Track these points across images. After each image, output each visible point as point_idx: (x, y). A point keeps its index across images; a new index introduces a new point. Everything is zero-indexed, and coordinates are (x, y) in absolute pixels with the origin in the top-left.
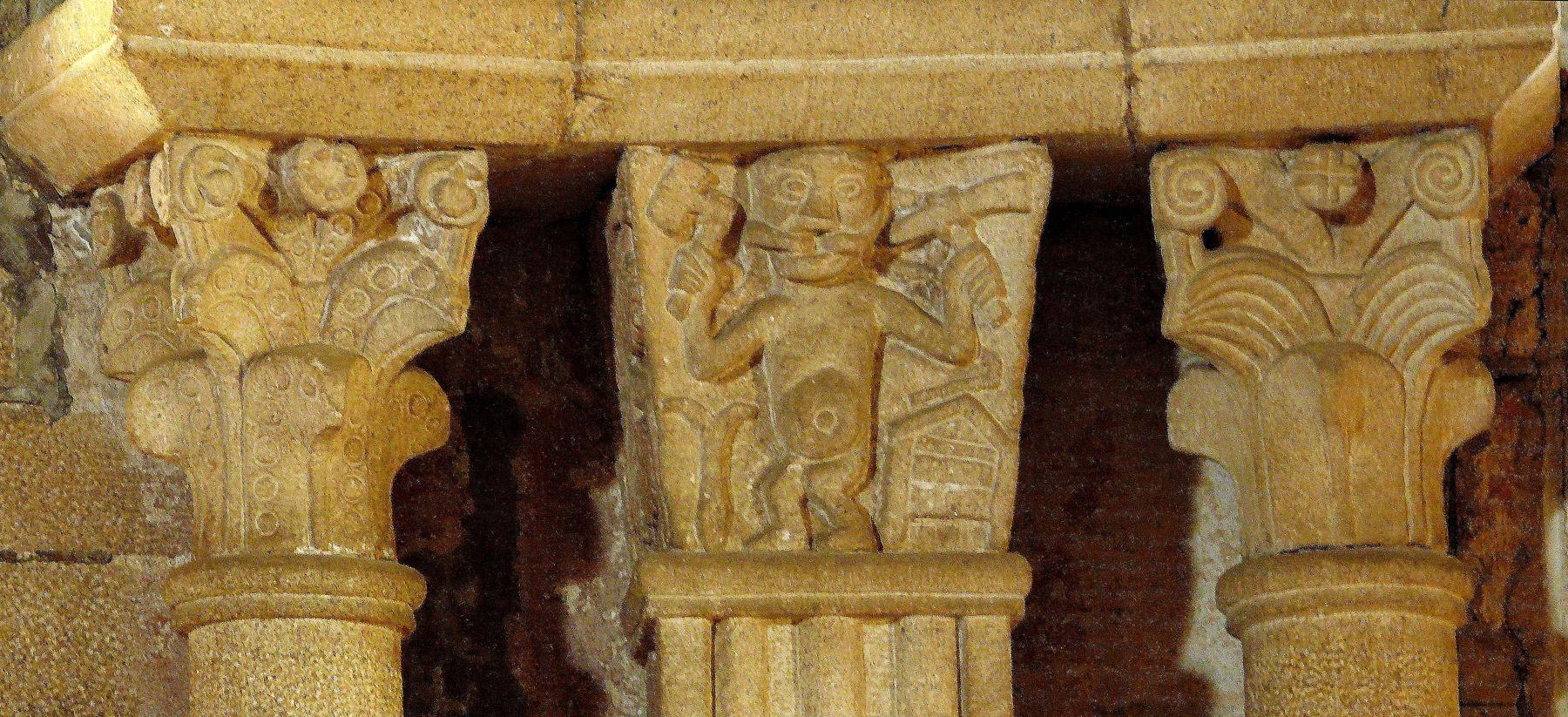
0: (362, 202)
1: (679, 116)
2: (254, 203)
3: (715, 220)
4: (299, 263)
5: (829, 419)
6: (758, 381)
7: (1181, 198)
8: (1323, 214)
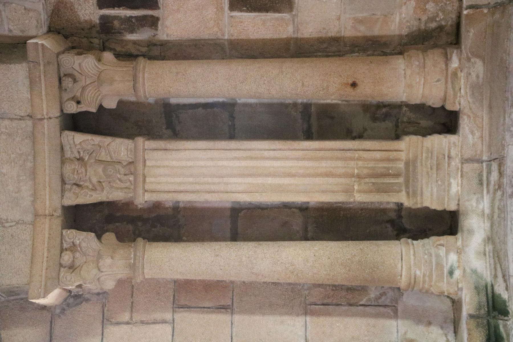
0: (72, 251)
1: (56, 198)
2: (71, 270)
3: (75, 189)
4: (82, 261)
5: (110, 170)
6: (104, 182)
7: (72, 108)
8: (74, 83)
